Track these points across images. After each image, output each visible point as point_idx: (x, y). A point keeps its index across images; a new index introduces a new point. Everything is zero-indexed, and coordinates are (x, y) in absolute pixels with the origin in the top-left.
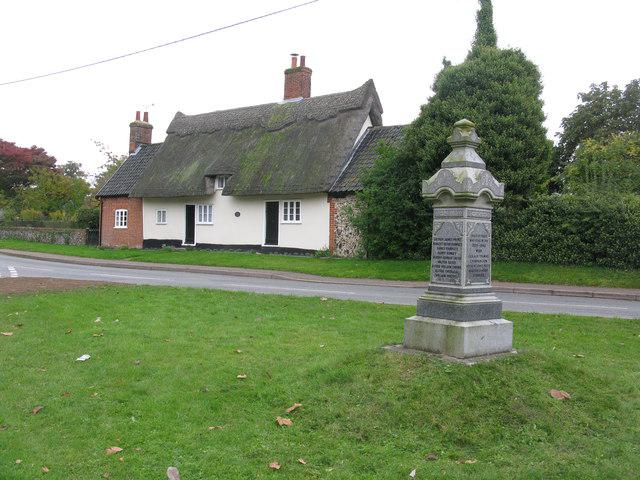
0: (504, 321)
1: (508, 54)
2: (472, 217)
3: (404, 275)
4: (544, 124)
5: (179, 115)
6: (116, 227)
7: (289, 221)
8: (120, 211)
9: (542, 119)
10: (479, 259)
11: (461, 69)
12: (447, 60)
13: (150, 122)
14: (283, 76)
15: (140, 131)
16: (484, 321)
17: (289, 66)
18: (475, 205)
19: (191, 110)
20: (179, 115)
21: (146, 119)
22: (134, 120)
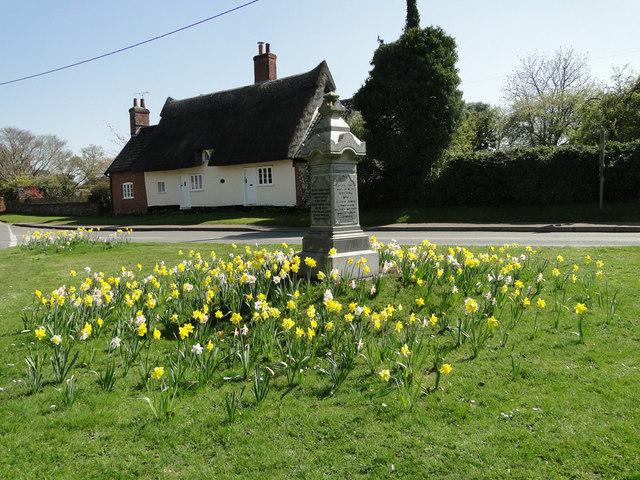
1: (429, 31)
4: (460, 88)
5: (169, 99)
11: (391, 46)
15: (137, 113)
17: (257, 54)
20: (169, 99)
21: (142, 105)
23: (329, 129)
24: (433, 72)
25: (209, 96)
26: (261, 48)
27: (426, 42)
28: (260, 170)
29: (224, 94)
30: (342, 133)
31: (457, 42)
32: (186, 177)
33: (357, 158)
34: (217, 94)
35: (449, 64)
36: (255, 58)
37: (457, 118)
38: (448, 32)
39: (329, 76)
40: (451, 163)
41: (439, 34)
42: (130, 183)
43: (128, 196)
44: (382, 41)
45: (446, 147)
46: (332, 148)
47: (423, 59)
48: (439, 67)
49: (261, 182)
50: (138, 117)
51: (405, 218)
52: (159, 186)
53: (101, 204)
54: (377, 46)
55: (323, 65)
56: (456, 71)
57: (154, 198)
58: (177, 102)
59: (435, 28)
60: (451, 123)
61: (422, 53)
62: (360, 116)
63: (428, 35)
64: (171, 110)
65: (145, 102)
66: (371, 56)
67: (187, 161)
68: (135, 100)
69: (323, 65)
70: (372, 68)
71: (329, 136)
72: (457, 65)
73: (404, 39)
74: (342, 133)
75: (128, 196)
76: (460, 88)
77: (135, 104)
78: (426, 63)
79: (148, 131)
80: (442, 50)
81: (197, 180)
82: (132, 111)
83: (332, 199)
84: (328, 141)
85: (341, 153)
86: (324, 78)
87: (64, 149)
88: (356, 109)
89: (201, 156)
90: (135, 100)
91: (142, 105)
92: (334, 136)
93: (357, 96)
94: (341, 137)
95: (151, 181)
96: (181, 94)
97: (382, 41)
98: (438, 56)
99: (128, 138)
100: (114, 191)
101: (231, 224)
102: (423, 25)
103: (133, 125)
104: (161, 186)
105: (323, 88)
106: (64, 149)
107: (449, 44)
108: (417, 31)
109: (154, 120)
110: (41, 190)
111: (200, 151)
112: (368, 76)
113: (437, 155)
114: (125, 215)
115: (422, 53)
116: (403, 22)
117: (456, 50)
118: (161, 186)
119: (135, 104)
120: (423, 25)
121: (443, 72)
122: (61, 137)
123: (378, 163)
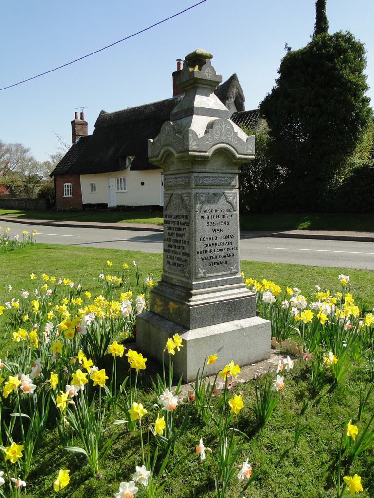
0: (257, 321)
1: (337, 36)
2: (205, 186)
3: (194, 242)
4: (367, 94)
5: (103, 112)
6: (65, 196)
7: (120, 191)
8: (66, 184)
9: (365, 88)
10: (218, 241)
11: (301, 53)
12: (289, 46)
13: (86, 120)
14: (172, 77)
15: (77, 125)
16: (212, 327)
17: (176, 70)
18: (208, 168)
19: (111, 110)
20: (103, 112)
21: (82, 118)
22: (73, 119)
23: (190, 111)
24: (342, 77)
25: (134, 109)
26: (179, 64)
27: (335, 47)
28: (118, 180)
29: (147, 106)
30: (211, 119)
31: (366, 47)
32: (112, 179)
33: (244, 166)
34: (140, 108)
35: (358, 70)
36: (174, 74)
37: (363, 124)
38: (357, 38)
39: (239, 89)
40: (356, 171)
41: (348, 39)
42: (69, 184)
43: (68, 195)
44: (289, 49)
45: (351, 154)
46: (193, 145)
47: (330, 64)
48: (346, 72)
49: (118, 189)
50: (78, 128)
51: (307, 224)
52: (92, 187)
53: (48, 200)
54: (284, 54)
55: (234, 78)
56: (364, 77)
57: (88, 198)
58: (109, 114)
59: (344, 33)
60: (356, 130)
61: (331, 58)
62: (266, 124)
63: (337, 40)
64: (104, 121)
65: (85, 116)
66: (278, 65)
67: (114, 166)
68: (76, 114)
69: (234, 78)
70: (278, 76)
71: (189, 124)
72: (365, 72)
73: (312, 45)
74: (211, 119)
75: (68, 195)
76: (367, 94)
77: (76, 117)
78: (334, 68)
79: (85, 139)
80: (351, 55)
81: (121, 182)
82: (73, 123)
83: (192, 233)
84: (184, 132)
85: (209, 154)
86: (234, 91)
87: (28, 155)
88: (261, 116)
89: (125, 161)
90: (76, 114)
91: (82, 118)
92: (198, 124)
93: (263, 105)
94: (211, 126)
95: (86, 182)
96: (112, 109)
97: (289, 49)
98: (346, 61)
99: (71, 145)
100: (57, 189)
101: (144, 223)
102: (331, 31)
103: (74, 135)
104: (93, 187)
105: (233, 100)
106: (28, 155)
107: (358, 49)
108: (325, 36)
109: (91, 130)
110: (8, 187)
111: (124, 158)
112: (275, 84)
113: (339, 163)
114: (65, 211)
115: (331, 58)
116: (312, 30)
117: (365, 56)
118: (93, 187)
119: (76, 117)
120: (331, 31)
121: (351, 77)
122: (26, 147)
123: (281, 170)
